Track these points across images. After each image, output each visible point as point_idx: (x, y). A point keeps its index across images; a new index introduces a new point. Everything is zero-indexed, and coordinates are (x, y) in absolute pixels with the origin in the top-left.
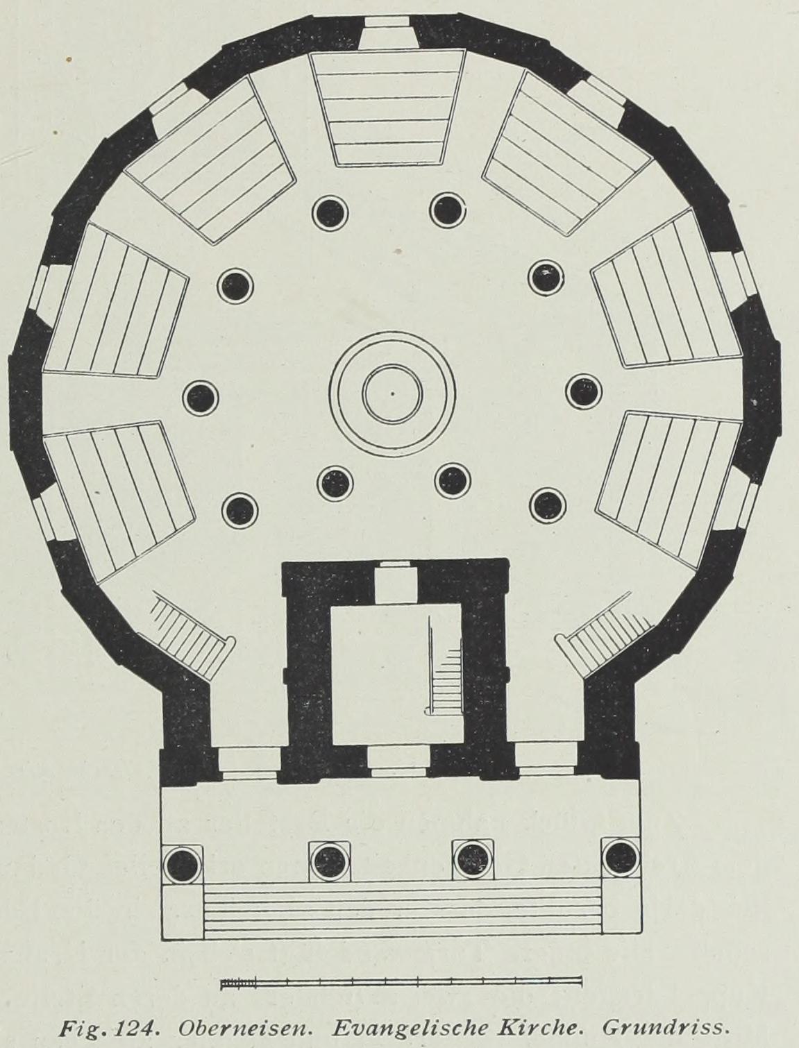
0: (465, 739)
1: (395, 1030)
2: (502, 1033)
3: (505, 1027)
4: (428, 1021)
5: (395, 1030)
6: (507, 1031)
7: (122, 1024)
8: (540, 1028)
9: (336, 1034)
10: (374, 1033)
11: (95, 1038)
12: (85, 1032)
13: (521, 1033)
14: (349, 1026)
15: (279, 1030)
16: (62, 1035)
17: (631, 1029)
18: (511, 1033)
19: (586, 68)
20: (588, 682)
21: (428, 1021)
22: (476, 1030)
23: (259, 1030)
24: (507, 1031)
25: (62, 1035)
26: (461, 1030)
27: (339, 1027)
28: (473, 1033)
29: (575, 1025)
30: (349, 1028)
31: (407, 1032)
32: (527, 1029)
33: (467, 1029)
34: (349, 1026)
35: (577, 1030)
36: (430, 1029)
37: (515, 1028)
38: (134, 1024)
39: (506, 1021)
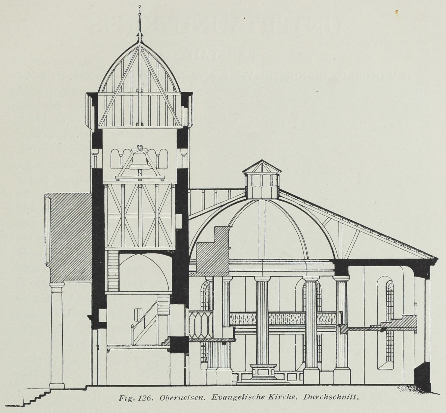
0: (348, 269)
1: (233, 398)
2: (269, 399)
3: (270, 397)
4: (244, 395)
5: (233, 398)
6: (271, 398)
7: (141, 396)
8: (282, 397)
9: (213, 399)
10: (226, 399)
11: (131, 401)
12: (128, 399)
13: (276, 399)
14: (217, 396)
15: (252, 397)
16: (120, 400)
17: (177, 399)
18: (272, 399)
19: (432, 380)
20: (416, 370)
21: (244, 395)
22: (291, 397)
23: (187, 398)
24: (271, 398)
25: (120, 400)
26: (336, 397)
27: (214, 397)
28: (259, 399)
29: (264, 396)
30: (217, 397)
31: (237, 398)
32: (278, 398)
33: (338, 397)
34: (217, 396)
35: (295, 398)
36: (245, 397)
37: (274, 397)
38: (145, 397)
39: (271, 395)
